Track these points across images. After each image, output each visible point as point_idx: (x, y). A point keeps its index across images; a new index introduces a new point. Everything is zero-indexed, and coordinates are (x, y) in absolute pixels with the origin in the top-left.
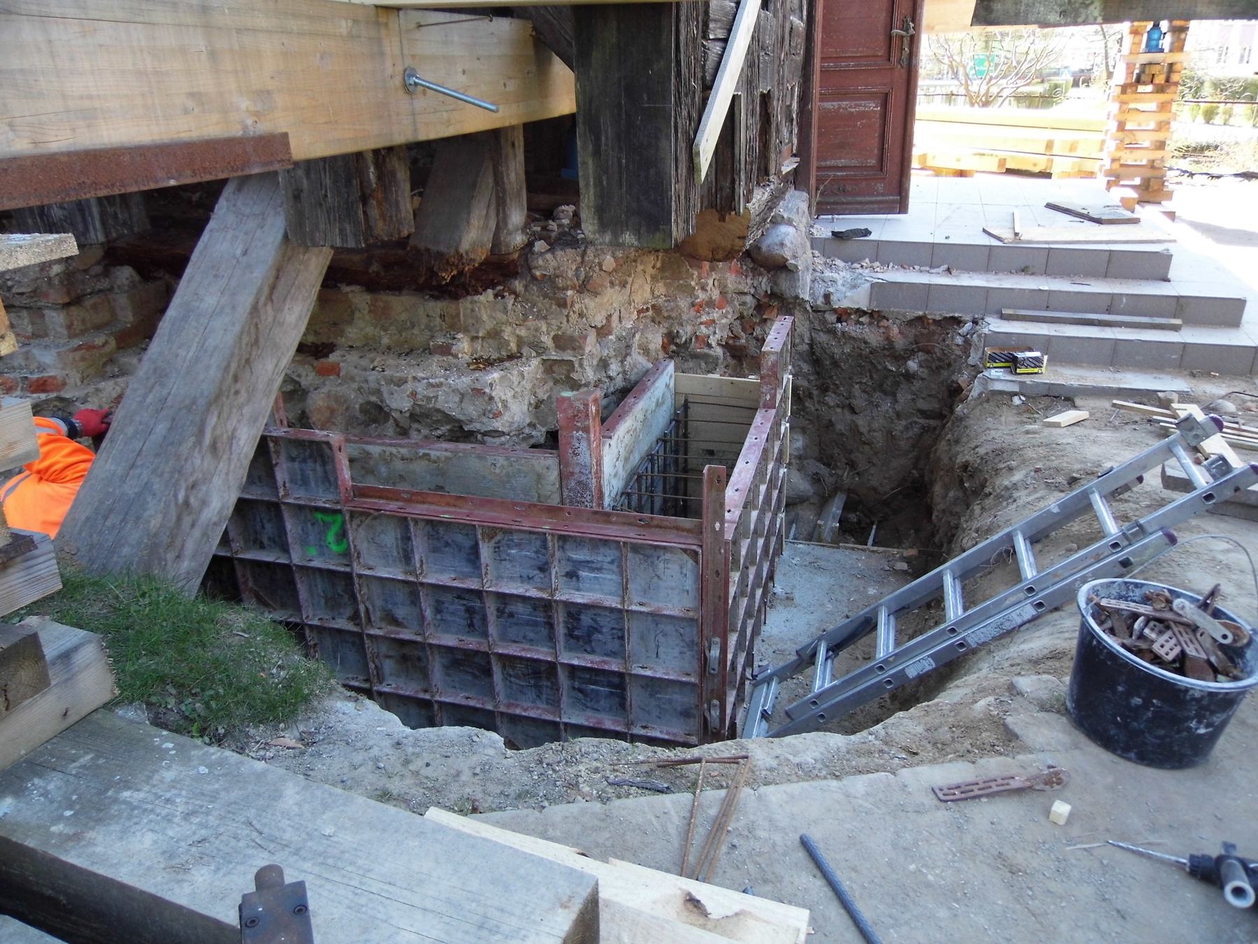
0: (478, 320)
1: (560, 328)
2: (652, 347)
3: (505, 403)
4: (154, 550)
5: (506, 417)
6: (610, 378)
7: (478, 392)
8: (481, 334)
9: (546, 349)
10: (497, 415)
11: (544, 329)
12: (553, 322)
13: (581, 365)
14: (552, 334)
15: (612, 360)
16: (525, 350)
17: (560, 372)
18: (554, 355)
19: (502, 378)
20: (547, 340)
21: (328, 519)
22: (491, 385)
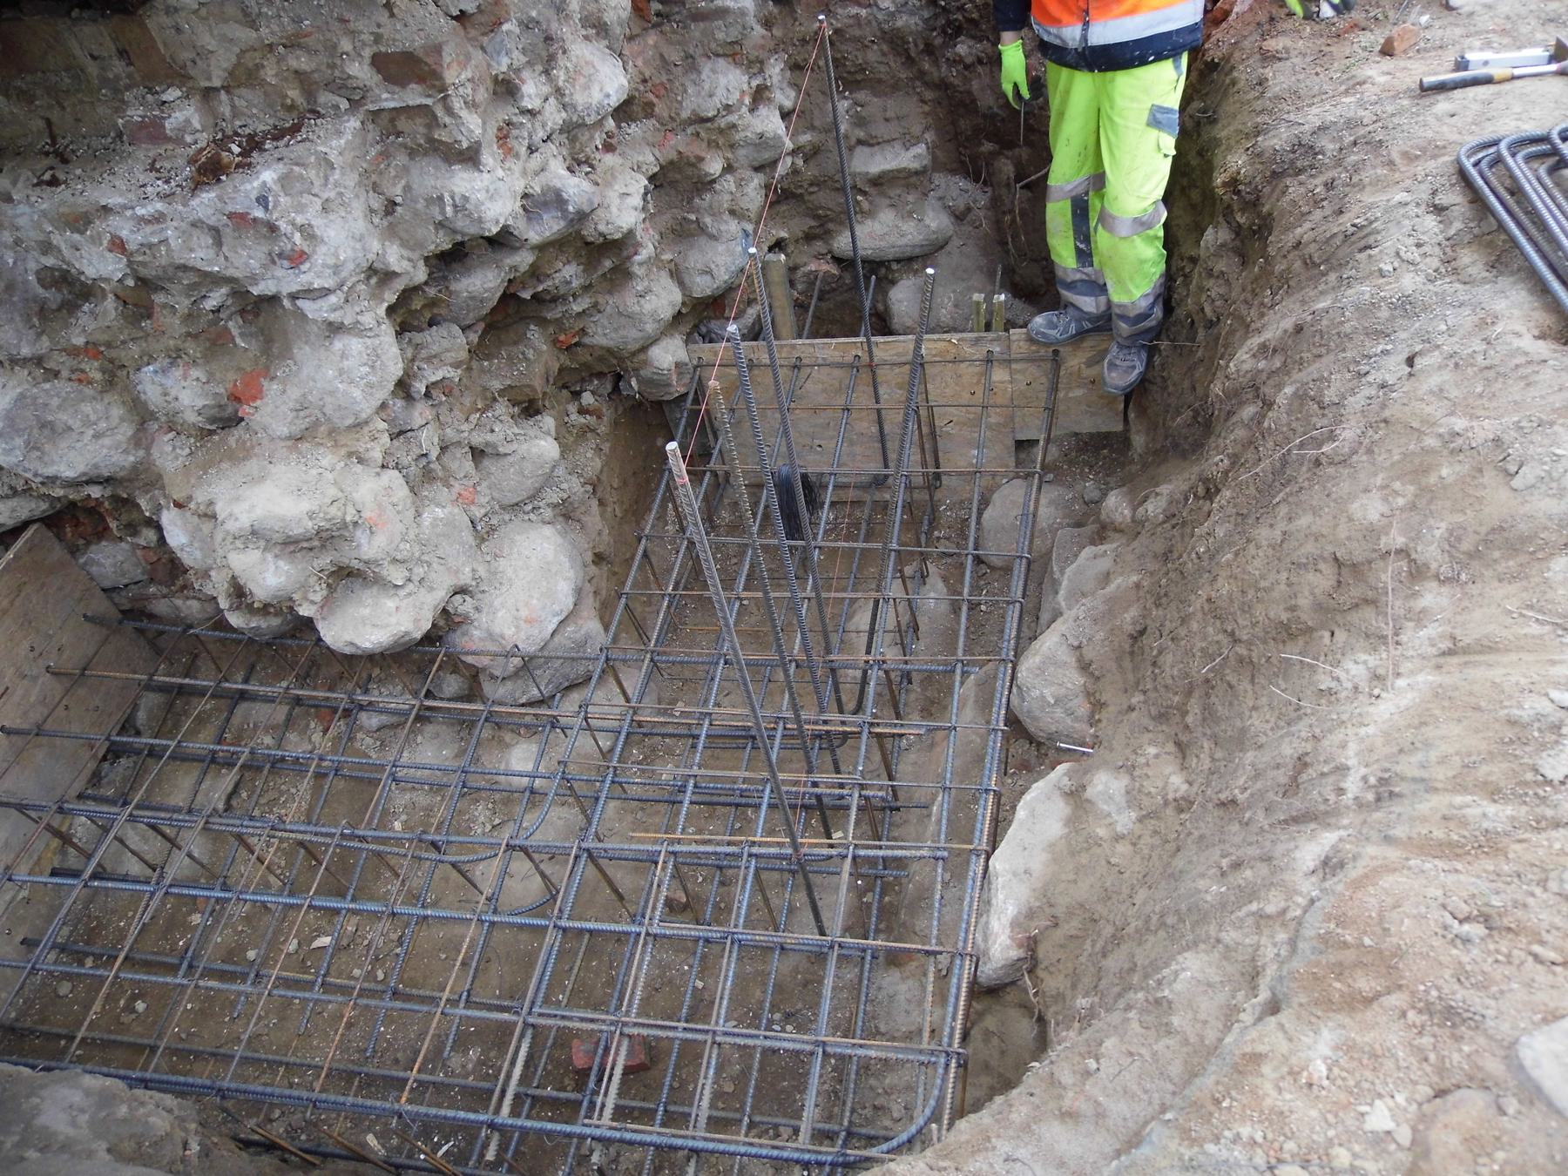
0: (203, 54)
1: (378, 38)
2: (609, 17)
3: (307, 231)
4: (1296, 97)
5: (321, 256)
6: (532, 113)
7: (240, 220)
8: (217, 83)
9: (366, 90)
10: (297, 259)
11: (346, 45)
12: (360, 25)
13: (449, 111)
14: (367, 53)
15: (526, 74)
16: (325, 98)
17: (415, 129)
18: (389, 99)
19: (284, 181)
20: (360, 71)
21: (218, 965)
22: (262, 201)
